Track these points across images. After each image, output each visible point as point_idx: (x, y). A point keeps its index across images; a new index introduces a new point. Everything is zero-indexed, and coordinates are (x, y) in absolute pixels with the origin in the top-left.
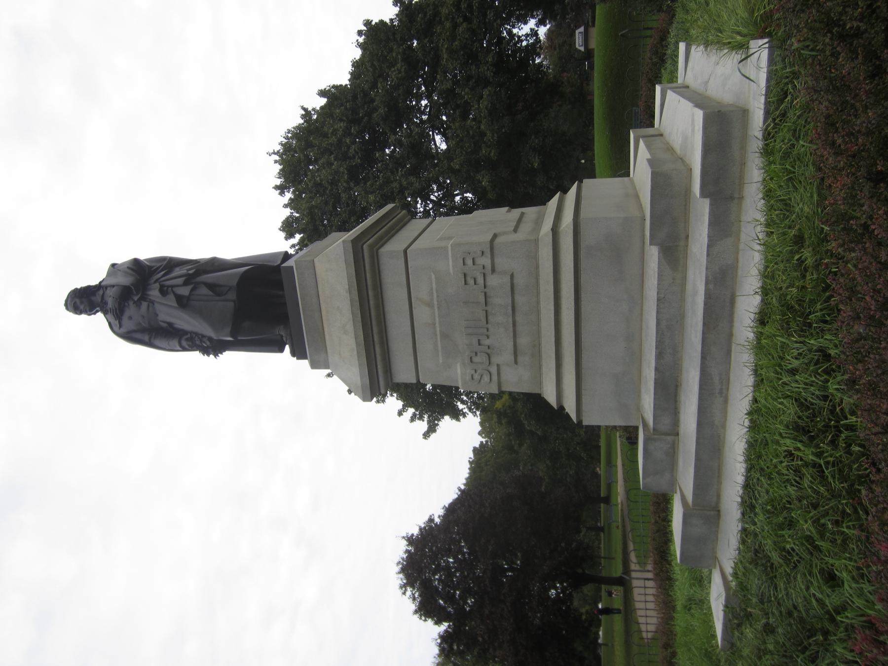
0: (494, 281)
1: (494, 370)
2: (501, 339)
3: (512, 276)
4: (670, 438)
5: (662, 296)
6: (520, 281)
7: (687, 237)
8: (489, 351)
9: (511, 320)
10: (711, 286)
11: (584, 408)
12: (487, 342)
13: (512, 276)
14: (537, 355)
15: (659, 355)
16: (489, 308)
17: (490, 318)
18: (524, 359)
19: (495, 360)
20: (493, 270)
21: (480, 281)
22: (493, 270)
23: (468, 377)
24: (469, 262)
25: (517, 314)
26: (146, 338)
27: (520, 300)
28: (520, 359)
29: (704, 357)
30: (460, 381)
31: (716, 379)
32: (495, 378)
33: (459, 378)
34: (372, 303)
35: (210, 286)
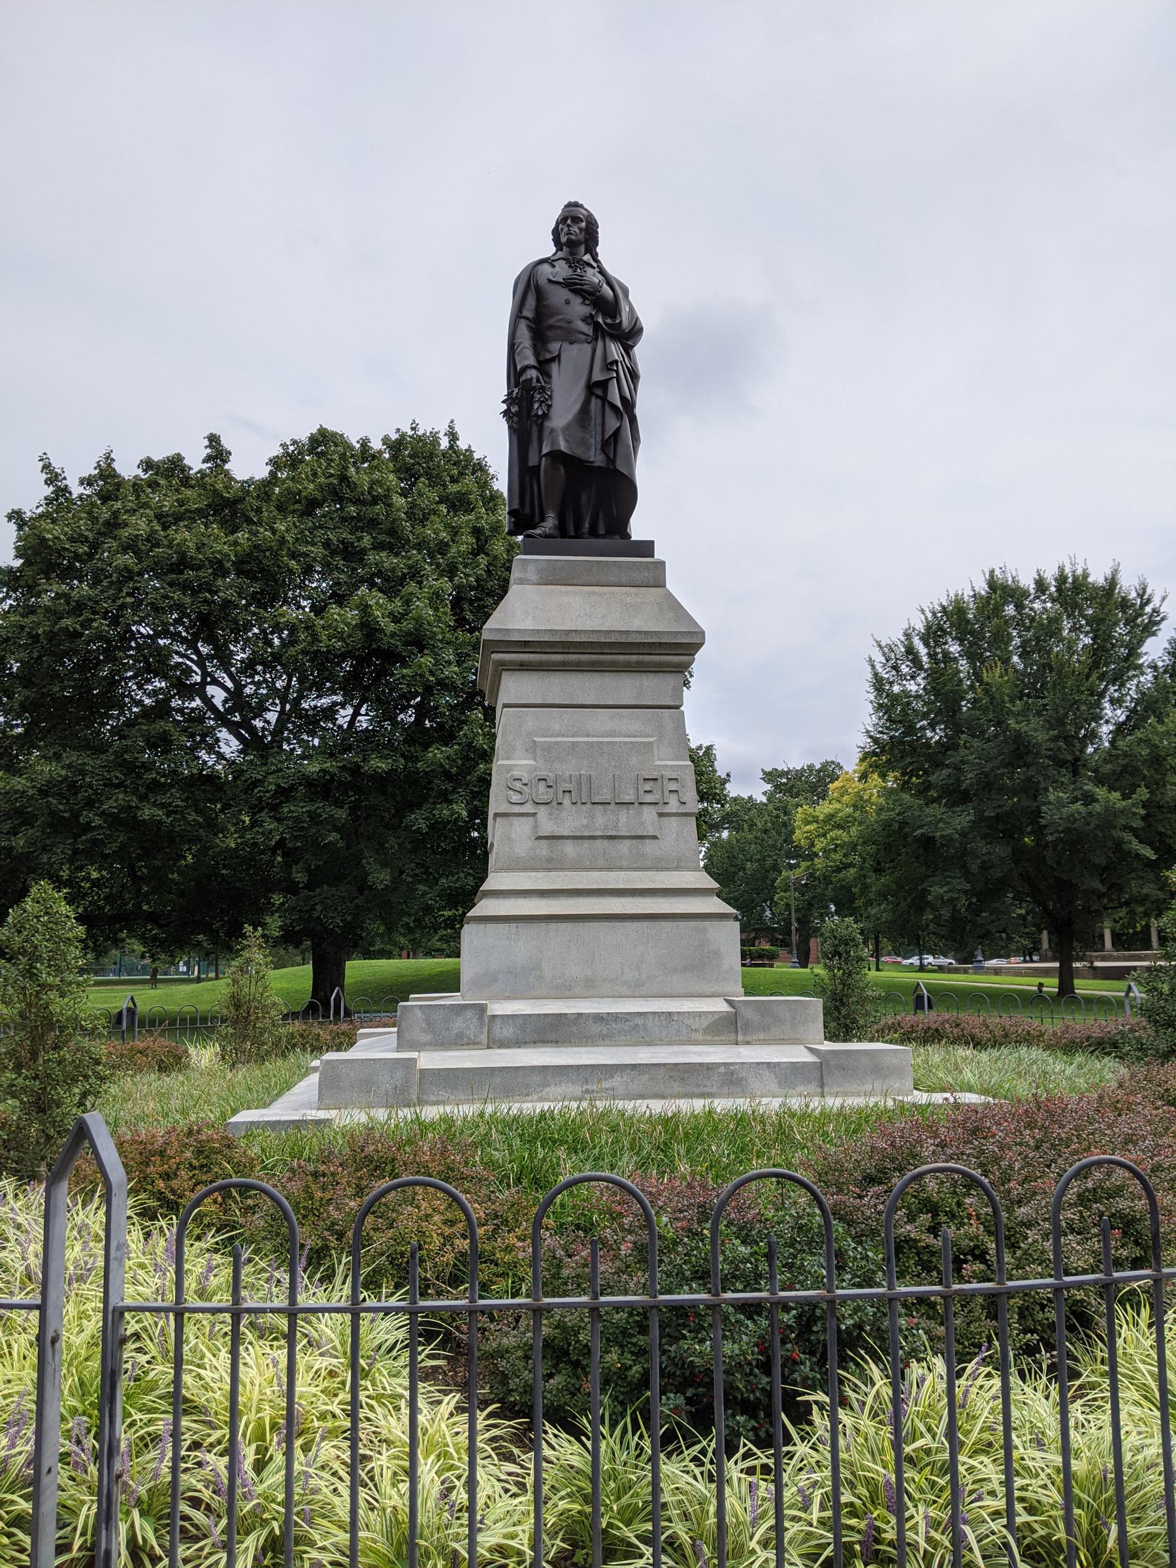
0: (649, 814)
1: (528, 808)
2: (571, 821)
3: (655, 837)
4: (484, 1038)
5: (675, 1018)
6: (649, 847)
7: (748, 1043)
8: (554, 804)
9: (599, 833)
10: (722, 1070)
11: (491, 927)
12: (567, 802)
13: (655, 837)
14: (550, 865)
15: (598, 1018)
16: (613, 806)
17: (600, 807)
18: (544, 849)
19: (542, 812)
20: (661, 815)
21: (649, 798)
22: (661, 815)
23: (516, 773)
24: (673, 786)
25: (606, 841)
26: (528, 313)
27: (624, 847)
28: (544, 843)
29: (634, 1067)
30: (505, 762)
31: (606, 1084)
32: (517, 809)
33: (513, 762)
34: (621, 657)
35: (617, 433)
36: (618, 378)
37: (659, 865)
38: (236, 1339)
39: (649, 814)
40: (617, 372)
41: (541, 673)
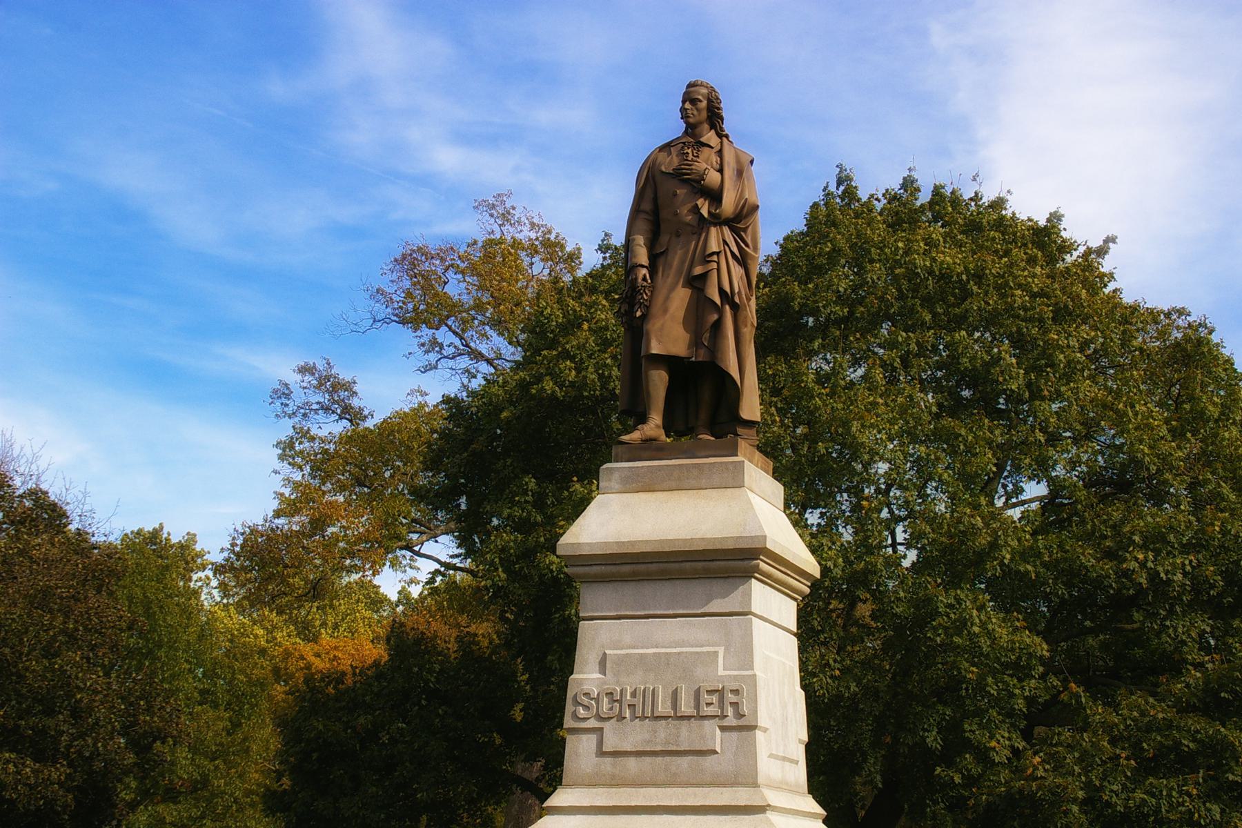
1: (592, 723)
9: (659, 748)
36: (718, 270)
37: (718, 782)
38: (419, 554)
39: (711, 727)
40: (718, 263)
41: (616, 584)
